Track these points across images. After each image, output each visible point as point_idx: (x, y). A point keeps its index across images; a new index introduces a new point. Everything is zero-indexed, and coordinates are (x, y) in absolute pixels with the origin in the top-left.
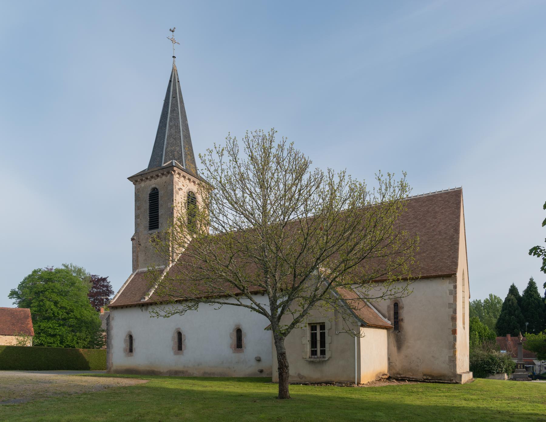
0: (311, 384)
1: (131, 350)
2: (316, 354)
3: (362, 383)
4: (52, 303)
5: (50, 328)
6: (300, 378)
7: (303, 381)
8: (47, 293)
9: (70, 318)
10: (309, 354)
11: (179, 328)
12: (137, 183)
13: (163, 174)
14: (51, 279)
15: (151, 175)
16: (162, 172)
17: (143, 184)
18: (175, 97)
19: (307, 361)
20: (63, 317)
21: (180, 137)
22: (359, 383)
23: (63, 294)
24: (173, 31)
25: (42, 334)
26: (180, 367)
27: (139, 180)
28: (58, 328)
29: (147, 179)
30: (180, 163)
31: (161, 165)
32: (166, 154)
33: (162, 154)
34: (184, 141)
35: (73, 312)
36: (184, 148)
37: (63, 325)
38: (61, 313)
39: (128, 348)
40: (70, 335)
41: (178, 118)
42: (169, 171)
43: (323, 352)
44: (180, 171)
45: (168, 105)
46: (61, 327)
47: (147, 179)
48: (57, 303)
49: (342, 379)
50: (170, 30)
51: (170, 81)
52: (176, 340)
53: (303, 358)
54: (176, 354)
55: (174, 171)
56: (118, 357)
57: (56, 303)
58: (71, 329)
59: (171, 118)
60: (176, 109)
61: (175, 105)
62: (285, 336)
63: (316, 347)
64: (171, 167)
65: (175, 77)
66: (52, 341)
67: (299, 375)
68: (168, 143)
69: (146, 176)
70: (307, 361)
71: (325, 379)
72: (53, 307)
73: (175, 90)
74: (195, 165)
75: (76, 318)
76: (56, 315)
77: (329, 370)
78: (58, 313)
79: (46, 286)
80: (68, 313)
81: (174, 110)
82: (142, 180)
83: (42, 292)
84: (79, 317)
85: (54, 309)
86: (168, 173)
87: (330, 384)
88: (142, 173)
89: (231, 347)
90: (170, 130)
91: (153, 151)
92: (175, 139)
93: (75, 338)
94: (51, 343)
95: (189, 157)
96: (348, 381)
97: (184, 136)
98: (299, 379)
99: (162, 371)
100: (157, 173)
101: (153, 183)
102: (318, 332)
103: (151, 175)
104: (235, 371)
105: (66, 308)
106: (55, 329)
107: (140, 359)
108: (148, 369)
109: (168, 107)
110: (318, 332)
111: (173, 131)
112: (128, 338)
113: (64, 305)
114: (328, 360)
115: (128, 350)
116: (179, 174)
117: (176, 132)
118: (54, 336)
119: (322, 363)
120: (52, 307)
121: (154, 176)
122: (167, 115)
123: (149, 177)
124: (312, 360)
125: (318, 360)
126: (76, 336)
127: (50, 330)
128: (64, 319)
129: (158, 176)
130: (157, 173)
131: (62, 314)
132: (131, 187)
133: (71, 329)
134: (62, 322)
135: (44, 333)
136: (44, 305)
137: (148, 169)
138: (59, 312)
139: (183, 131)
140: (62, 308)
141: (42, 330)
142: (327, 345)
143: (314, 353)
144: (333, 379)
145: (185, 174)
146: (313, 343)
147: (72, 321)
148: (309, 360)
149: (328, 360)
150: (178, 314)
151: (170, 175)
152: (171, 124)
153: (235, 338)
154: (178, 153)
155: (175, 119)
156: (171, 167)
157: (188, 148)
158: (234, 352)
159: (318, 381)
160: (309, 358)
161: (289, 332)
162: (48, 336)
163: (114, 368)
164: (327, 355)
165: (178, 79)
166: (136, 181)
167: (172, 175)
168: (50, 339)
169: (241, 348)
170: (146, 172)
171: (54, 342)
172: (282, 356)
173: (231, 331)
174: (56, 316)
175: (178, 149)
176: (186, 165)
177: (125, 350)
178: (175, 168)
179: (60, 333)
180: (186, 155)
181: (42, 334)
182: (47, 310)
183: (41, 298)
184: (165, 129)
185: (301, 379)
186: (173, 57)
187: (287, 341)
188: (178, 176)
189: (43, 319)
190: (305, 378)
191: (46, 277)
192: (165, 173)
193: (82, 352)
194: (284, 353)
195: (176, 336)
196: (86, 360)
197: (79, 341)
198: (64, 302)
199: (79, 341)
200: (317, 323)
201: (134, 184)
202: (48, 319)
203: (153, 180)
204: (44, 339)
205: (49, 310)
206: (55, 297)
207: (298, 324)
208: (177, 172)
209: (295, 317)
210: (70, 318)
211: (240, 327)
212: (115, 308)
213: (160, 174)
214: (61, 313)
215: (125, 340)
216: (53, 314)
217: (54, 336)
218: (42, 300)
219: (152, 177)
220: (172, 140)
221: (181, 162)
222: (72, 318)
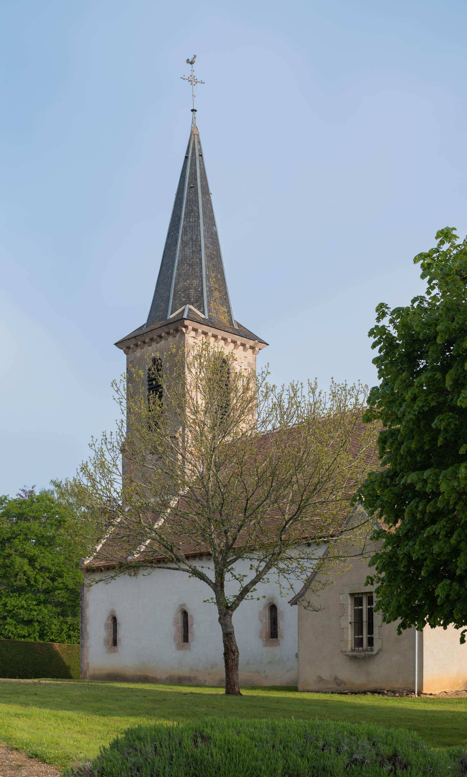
0: (352, 693)
1: (115, 643)
2: (362, 646)
3: (424, 691)
4: (26, 561)
5: (22, 607)
6: (337, 684)
7: (341, 688)
8: (16, 541)
9: (57, 589)
10: (350, 645)
11: (184, 605)
12: (130, 350)
13: (168, 333)
14: (23, 514)
15: (151, 335)
16: (167, 330)
17: (138, 353)
18: (193, 187)
19: (347, 655)
20: (45, 587)
21: (201, 260)
22: (420, 693)
23: (45, 542)
24: (192, 63)
25: (9, 620)
26: (185, 672)
27: (132, 346)
28: (36, 608)
29: (144, 343)
30: (199, 309)
31: (166, 316)
32: (174, 296)
33: (169, 297)
34: (207, 267)
35: (61, 577)
36: (208, 279)
37: (45, 602)
38: (41, 580)
39: (111, 638)
40: (55, 621)
41: (198, 226)
42: (176, 328)
43: (371, 642)
44: (197, 325)
45: (182, 203)
46: (41, 607)
47: (144, 343)
48: (35, 561)
49: (397, 686)
50: (188, 61)
51: (186, 157)
52: (180, 624)
53: (342, 651)
54: (180, 648)
55: (186, 327)
56: (96, 655)
57: (32, 560)
58: (59, 610)
59: (185, 228)
60: (195, 208)
61: (193, 202)
62: (233, 611)
63: (362, 634)
64: (180, 320)
65: (194, 149)
66: (25, 632)
67: (336, 678)
68: (179, 275)
69: (142, 338)
70: (347, 655)
71: (372, 686)
72: (26, 568)
73: (194, 173)
74: (229, 307)
75: (67, 588)
76: (32, 582)
77: (380, 670)
78: (36, 580)
79: (15, 528)
80: (53, 580)
81: (192, 211)
82: (136, 345)
83: (8, 540)
84: (71, 586)
85: (29, 573)
86: (177, 330)
87: (379, 693)
88: (137, 333)
89: (261, 637)
90: (183, 249)
91: (156, 291)
92: (191, 265)
93: (65, 627)
94: (24, 637)
95: (216, 294)
96: (404, 689)
97: (207, 256)
98: (336, 686)
99: (159, 677)
100: (159, 332)
101: (151, 351)
102: (365, 607)
103: (151, 335)
104: (266, 677)
105: (49, 571)
106: (31, 610)
107: (125, 659)
108: (139, 674)
109: (182, 207)
110: (365, 607)
111: (188, 251)
112: (110, 622)
113: (46, 564)
114: (378, 653)
115: (111, 642)
116: (195, 330)
117: (193, 252)
118: (29, 623)
119: (369, 658)
120: (25, 569)
121: (155, 337)
122: (179, 223)
123: (147, 340)
124: (354, 654)
125: (363, 654)
126: (66, 623)
127: (22, 611)
128: (47, 591)
129: (160, 337)
130: (159, 332)
131: (43, 582)
132: (121, 357)
133: (59, 610)
134: (42, 597)
135: (12, 618)
136: (12, 564)
137: (147, 324)
138: (38, 577)
139: (206, 247)
140: (42, 569)
141: (10, 611)
142: (376, 630)
143: (359, 642)
144: (384, 686)
145: (206, 328)
146: (358, 629)
147: (61, 596)
148: (351, 654)
149: (378, 653)
150: (103, 582)
151: (179, 334)
152: (185, 238)
153: (267, 620)
154: (196, 290)
155: (193, 228)
156: (180, 320)
157: (216, 276)
158: (265, 645)
159: (363, 689)
160: (353, 651)
161: (237, 605)
162: (19, 623)
163: (90, 672)
164: (376, 646)
165: (200, 150)
166: (129, 348)
167: (183, 334)
168: (23, 629)
169: (277, 637)
170: (145, 330)
171: (30, 635)
172: (228, 636)
173: (261, 609)
174: (33, 586)
175: (196, 282)
176: (209, 311)
177: (106, 642)
178: (187, 323)
179: (40, 618)
180: (210, 291)
181: (9, 620)
182: (17, 575)
183: (7, 551)
184: (175, 250)
185: (339, 685)
186: (193, 110)
187: (237, 618)
188: (193, 334)
189: (12, 592)
190: (345, 684)
191: (16, 511)
192: (172, 331)
193: (58, 649)
194: (231, 634)
195: (180, 616)
196: (64, 663)
197: (72, 633)
198: (46, 559)
199: (72, 633)
200: (362, 593)
201: (125, 352)
202: (20, 590)
203: (154, 345)
204: (12, 629)
205: (21, 575)
206: (31, 548)
207: (249, 594)
208: (190, 328)
209: (244, 586)
210: (57, 589)
211: (275, 602)
212: (90, 570)
213: (163, 334)
214: (41, 580)
215: (106, 625)
216: (28, 581)
217: (29, 623)
218: (9, 555)
219: (152, 340)
220: (186, 267)
221: (200, 307)
222: (61, 589)
